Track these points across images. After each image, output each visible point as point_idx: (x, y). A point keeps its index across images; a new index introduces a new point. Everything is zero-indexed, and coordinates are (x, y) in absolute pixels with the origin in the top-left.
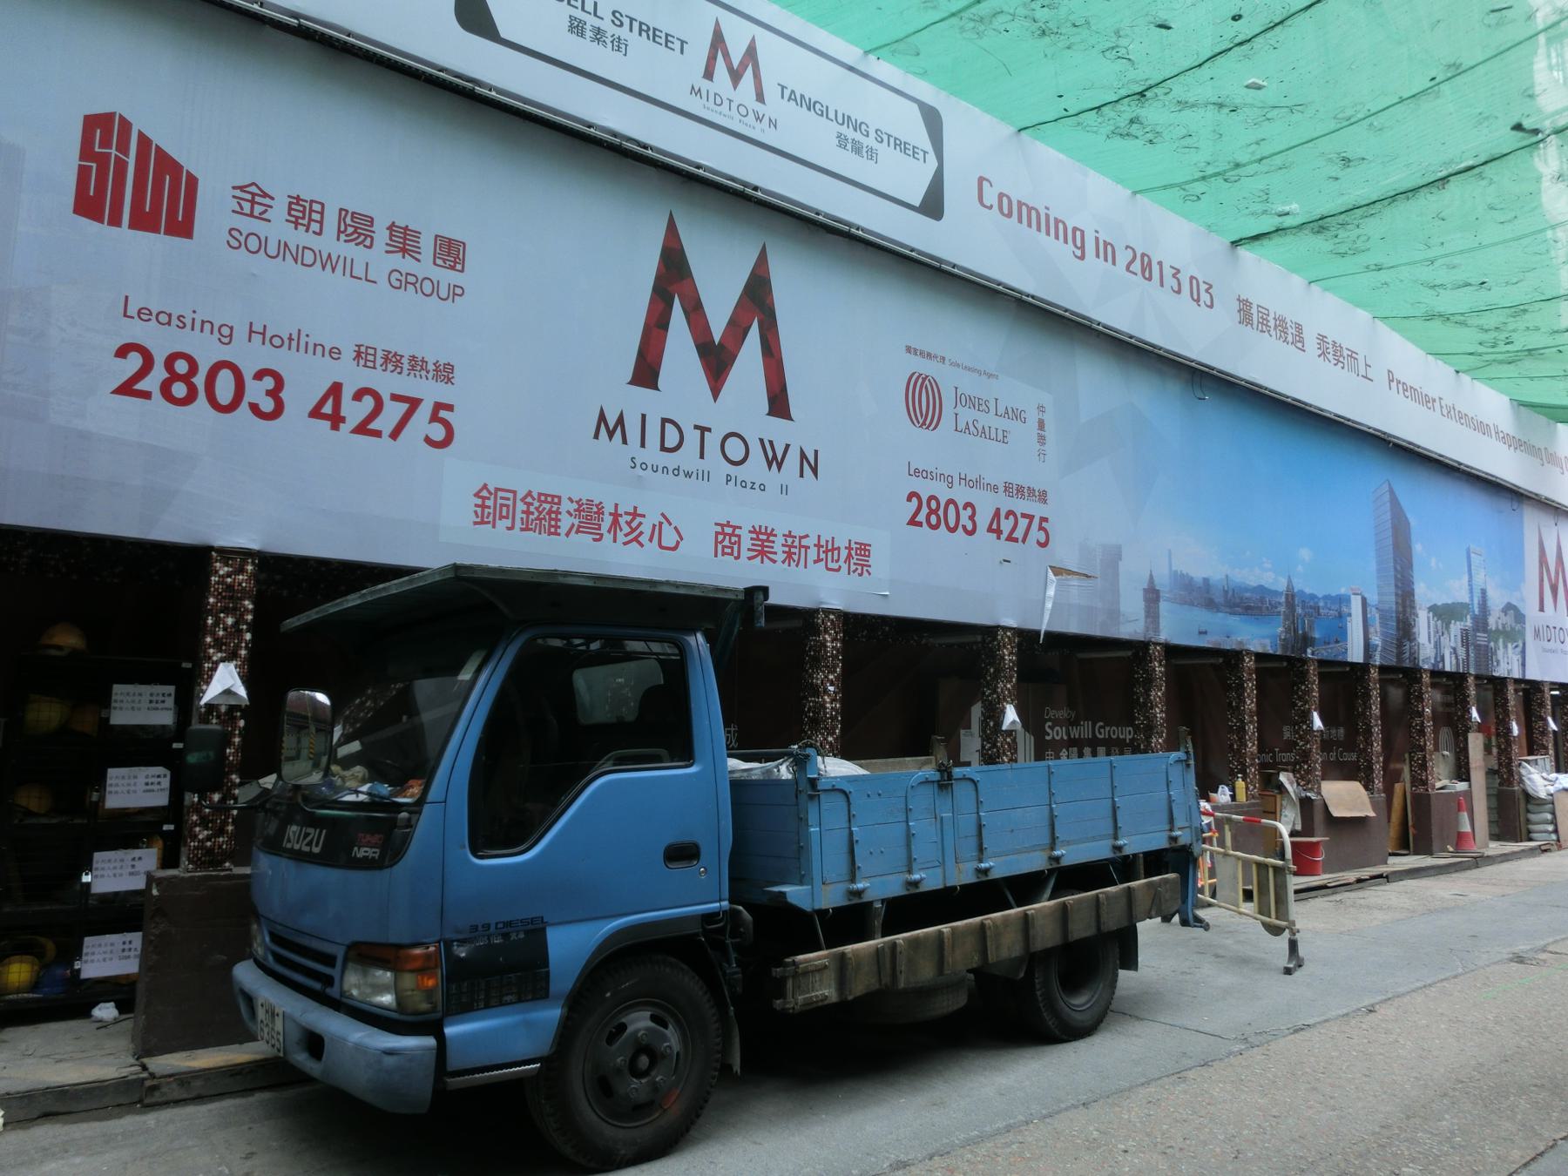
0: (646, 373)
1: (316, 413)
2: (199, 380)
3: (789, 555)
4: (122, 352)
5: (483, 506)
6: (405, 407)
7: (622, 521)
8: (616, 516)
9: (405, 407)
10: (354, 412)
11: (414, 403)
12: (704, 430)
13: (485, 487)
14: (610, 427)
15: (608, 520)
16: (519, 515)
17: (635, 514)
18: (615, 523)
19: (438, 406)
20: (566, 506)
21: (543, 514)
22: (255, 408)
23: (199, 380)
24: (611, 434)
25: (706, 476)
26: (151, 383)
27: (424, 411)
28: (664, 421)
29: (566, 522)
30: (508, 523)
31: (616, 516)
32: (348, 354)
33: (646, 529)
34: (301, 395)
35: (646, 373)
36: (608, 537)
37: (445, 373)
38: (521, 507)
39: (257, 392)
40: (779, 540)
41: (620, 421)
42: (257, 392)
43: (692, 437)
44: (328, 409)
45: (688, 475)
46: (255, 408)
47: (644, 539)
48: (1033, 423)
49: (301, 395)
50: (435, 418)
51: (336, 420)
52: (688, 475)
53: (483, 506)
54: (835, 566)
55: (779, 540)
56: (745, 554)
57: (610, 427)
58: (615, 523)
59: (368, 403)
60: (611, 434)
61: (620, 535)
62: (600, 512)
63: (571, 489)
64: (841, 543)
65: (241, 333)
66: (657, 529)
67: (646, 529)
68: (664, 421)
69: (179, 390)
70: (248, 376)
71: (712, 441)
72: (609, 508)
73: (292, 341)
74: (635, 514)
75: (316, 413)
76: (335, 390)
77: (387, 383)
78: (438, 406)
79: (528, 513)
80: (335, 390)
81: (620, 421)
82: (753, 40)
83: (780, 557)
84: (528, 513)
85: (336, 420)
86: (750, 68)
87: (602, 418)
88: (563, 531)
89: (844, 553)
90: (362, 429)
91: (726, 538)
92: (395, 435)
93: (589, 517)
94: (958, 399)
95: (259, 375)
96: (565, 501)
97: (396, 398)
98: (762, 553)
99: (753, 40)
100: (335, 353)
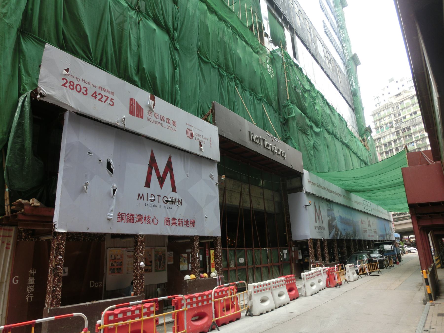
0: (148, 184)
1: (92, 96)
2: (75, 86)
3: (179, 224)
4: (63, 79)
5: (119, 218)
6: (106, 98)
7: (146, 218)
8: (145, 217)
9: (106, 98)
10: (99, 97)
11: (108, 98)
12: (159, 196)
13: (119, 213)
14: (141, 197)
15: (144, 218)
16: (126, 219)
17: (149, 217)
18: (145, 219)
19: (111, 99)
20: (135, 216)
21: (131, 218)
22: (83, 93)
23: (75, 86)
24: (141, 198)
25: (160, 206)
26: (68, 85)
27: (109, 99)
28: (151, 195)
29: (135, 220)
30: (124, 221)
31: (145, 217)
32: (97, 87)
33: (151, 220)
34: (90, 92)
35: (148, 184)
36: (144, 223)
37: (112, 94)
38: (126, 217)
39: (83, 90)
40: (177, 221)
41: (143, 195)
42: (83, 90)
43: (157, 198)
44: (94, 95)
45: (156, 206)
46: (83, 93)
47: (151, 222)
48: (209, 140)
49: (90, 92)
50: (111, 101)
51: (96, 98)
52: (156, 206)
53: (119, 218)
54: (188, 225)
55: (177, 221)
56: (171, 224)
57: (141, 197)
58: (145, 219)
59: (100, 96)
60: (141, 198)
61: (146, 222)
62: (142, 217)
63: (136, 212)
64: (189, 220)
65: (81, 80)
66: (153, 220)
67: (151, 220)
68: (151, 195)
69: (71, 87)
70: (82, 87)
71: (161, 198)
72: (144, 216)
73: (89, 83)
74: (149, 217)
75: (92, 96)
76: (95, 93)
77: (103, 93)
78: (111, 99)
79: (128, 218)
80: (95, 93)
81: (143, 195)
82: (161, 187)
83: (177, 224)
84: (128, 218)
85: (96, 98)
86: (161, 175)
87: (139, 195)
88: (135, 222)
89: (190, 222)
90: (99, 100)
91: (167, 221)
92: (105, 102)
93: (140, 218)
94: (195, 134)
95: (84, 87)
96: (135, 215)
97: (105, 96)
98: (174, 224)
99: (161, 187)
100: (95, 86)
